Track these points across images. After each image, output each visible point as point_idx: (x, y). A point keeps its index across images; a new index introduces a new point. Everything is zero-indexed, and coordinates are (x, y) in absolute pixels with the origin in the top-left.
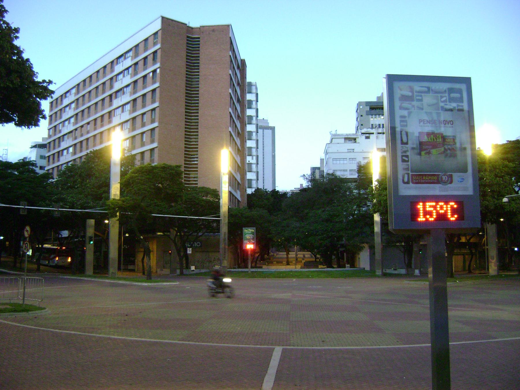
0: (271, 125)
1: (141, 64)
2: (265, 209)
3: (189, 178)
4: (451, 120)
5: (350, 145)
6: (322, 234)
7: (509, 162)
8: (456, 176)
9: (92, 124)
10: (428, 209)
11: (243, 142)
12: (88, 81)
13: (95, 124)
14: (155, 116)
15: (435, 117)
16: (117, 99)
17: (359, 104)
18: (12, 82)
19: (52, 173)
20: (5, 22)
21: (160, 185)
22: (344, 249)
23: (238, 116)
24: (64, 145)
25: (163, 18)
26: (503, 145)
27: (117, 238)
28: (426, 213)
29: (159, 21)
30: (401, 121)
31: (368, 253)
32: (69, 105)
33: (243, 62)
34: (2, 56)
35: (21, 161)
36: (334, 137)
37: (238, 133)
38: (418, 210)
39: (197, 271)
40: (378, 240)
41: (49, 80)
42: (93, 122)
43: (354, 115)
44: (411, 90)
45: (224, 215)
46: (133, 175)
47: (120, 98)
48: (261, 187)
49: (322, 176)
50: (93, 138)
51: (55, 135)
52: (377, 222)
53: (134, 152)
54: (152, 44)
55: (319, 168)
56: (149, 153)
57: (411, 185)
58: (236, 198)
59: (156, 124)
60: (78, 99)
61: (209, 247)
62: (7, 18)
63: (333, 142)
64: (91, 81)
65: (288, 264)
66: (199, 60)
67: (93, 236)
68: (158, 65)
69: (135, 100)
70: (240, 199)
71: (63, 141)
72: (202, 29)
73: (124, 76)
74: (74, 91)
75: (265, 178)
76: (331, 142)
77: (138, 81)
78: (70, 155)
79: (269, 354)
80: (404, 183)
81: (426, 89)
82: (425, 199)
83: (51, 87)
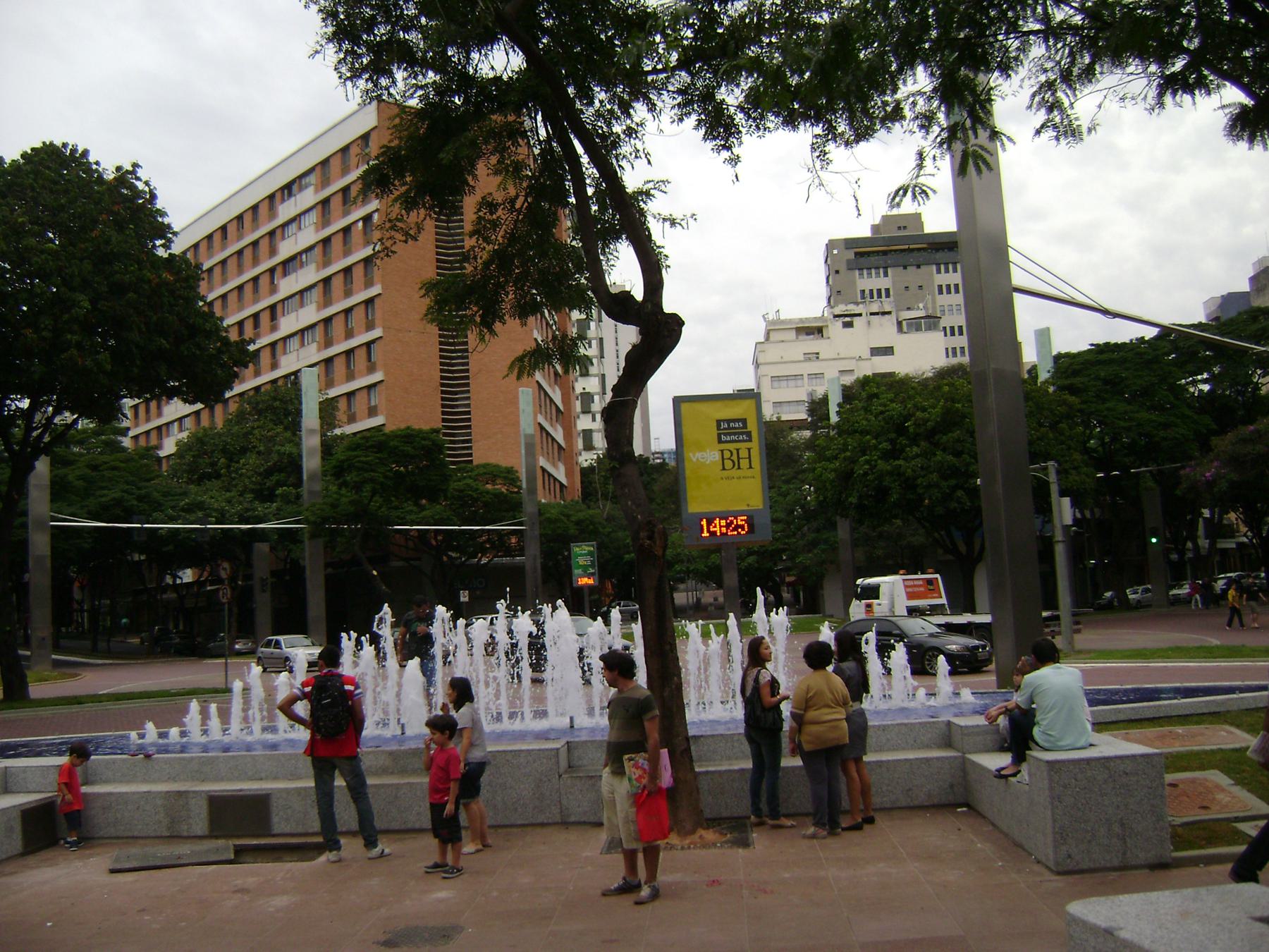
5: (812, 344)
16: (288, 278)
17: (831, 245)
36: (774, 328)
38: (702, 526)
43: (820, 272)
53: (333, 393)
58: (555, 479)
63: (772, 339)
70: (564, 481)
77: (261, 242)
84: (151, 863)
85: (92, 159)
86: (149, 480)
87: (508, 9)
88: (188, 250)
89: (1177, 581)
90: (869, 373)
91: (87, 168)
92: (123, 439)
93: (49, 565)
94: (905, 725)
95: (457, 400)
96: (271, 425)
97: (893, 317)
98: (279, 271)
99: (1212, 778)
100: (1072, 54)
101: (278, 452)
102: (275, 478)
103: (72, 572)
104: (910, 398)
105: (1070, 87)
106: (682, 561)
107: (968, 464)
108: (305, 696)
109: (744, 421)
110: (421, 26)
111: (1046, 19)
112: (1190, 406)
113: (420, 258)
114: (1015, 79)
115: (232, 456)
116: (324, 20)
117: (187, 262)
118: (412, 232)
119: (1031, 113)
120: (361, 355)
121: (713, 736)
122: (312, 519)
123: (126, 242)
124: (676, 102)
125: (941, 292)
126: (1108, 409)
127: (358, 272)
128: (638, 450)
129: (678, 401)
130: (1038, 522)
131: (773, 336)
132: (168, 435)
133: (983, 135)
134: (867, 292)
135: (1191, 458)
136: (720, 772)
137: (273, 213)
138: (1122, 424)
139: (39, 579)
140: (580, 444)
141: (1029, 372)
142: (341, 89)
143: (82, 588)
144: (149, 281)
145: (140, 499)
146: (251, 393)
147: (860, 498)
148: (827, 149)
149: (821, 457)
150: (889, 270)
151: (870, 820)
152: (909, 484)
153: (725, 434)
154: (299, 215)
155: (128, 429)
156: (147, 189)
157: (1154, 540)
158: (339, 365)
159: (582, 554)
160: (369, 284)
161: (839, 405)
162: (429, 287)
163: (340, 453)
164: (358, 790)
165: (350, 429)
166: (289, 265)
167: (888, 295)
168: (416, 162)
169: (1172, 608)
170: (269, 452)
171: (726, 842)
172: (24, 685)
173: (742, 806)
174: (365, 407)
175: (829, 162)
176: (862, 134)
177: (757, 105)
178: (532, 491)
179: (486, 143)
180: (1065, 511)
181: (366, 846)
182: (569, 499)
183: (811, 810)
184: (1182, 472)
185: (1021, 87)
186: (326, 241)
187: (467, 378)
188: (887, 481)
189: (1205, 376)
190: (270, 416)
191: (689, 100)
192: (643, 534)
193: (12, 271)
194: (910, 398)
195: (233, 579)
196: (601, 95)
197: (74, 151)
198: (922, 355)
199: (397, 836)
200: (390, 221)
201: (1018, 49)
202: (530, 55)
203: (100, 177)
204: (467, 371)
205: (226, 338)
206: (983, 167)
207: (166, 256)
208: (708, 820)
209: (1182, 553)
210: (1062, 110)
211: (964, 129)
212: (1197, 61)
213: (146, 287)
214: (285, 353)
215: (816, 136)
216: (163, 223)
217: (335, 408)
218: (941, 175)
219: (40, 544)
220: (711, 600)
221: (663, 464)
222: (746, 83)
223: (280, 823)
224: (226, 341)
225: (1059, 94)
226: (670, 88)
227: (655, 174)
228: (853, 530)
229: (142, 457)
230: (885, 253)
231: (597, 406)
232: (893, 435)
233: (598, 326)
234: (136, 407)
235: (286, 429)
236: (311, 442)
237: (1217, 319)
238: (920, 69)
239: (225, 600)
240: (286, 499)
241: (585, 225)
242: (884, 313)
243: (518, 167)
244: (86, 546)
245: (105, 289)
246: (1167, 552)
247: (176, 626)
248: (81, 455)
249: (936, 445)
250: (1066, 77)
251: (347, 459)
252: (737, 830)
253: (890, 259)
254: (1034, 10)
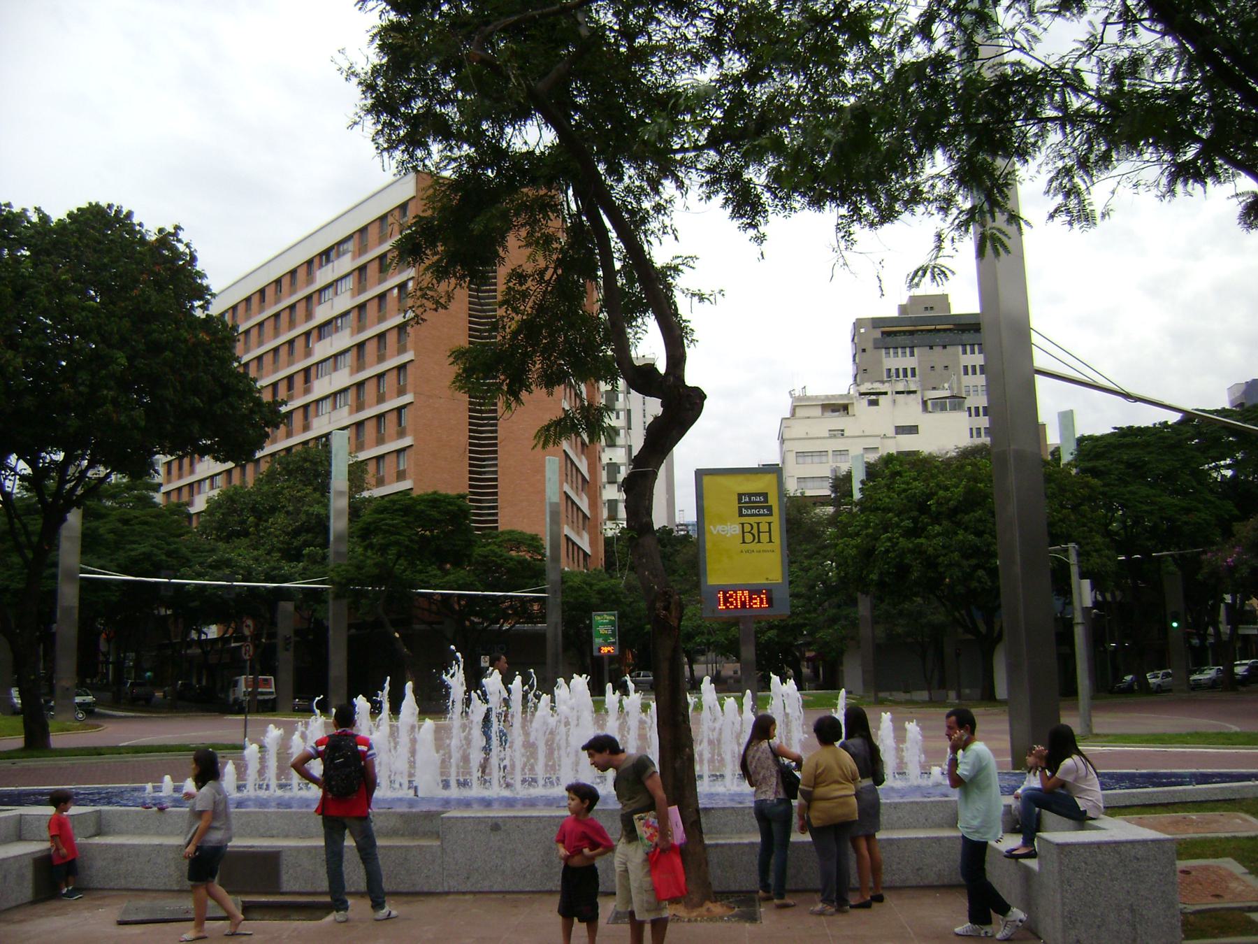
5: (837, 421)
14: (405, 380)
16: (323, 342)
17: (858, 324)
36: (800, 404)
43: (847, 349)
53: (362, 456)
58: (579, 548)
70: (588, 551)
76: (793, 414)
84: (159, 917)
85: (136, 220)
86: (182, 535)
87: (540, 86)
88: (226, 311)
89: (1199, 665)
90: (893, 451)
91: (131, 229)
92: (155, 495)
93: (76, 616)
94: (917, 803)
95: (484, 466)
96: (300, 486)
97: (918, 397)
98: (314, 334)
99: (1227, 866)
100: (1089, 141)
101: (307, 512)
102: (302, 538)
103: (99, 624)
104: (933, 476)
105: (1087, 173)
106: (703, 633)
107: (989, 545)
108: (319, 754)
109: (765, 495)
110: (458, 101)
111: (1063, 106)
112: (1211, 491)
113: (453, 325)
114: (1032, 165)
115: (261, 514)
116: (364, 92)
117: (225, 324)
118: (442, 301)
119: (1048, 198)
120: (391, 419)
121: (724, 809)
122: (337, 579)
123: (165, 302)
124: (703, 180)
125: (966, 373)
126: (1130, 492)
127: (392, 339)
128: (659, 520)
129: (700, 474)
130: (1058, 604)
131: (799, 412)
132: (199, 493)
133: (1001, 219)
134: (893, 371)
135: (1213, 544)
136: (730, 845)
137: (310, 278)
138: (1145, 508)
139: (66, 629)
140: (604, 476)
141: (1052, 454)
142: (378, 159)
143: (108, 640)
144: (186, 341)
145: (169, 554)
146: (282, 454)
147: (881, 574)
148: (852, 230)
149: (843, 533)
150: (916, 350)
151: (879, 899)
152: (930, 563)
153: (747, 508)
154: (337, 281)
155: (160, 485)
156: (187, 251)
157: (1175, 625)
158: (370, 429)
159: (603, 623)
160: (402, 350)
161: (862, 482)
162: (458, 355)
163: (367, 516)
164: (367, 851)
165: (378, 492)
166: (324, 329)
167: (913, 375)
168: (449, 232)
169: (1193, 693)
170: (298, 511)
171: (733, 916)
172: (45, 734)
173: (751, 881)
174: (393, 472)
175: (853, 243)
176: (887, 215)
177: (783, 185)
178: (556, 558)
179: (517, 214)
180: (1085, 593)
181: (373, 907)
182: (592, 567)
183: (820, 887)
184: (1204, 557)
185: (1038, 172)
186: (361, 307)
187: (495, 445)
188: (908, 560)
189: (1228, 461)
190: (299, 477)
191: (716, 178)
192: (659, 605)
193: (53, 327)
194: (933, 476)
195: (256, 637)
196: (630, 171)
197: (118, 212)
198: (947, 434)
199: (405, 899)
200: (421, 289)
201: (1036, 135)
202: (561, 132)
203: (143, 237)
204: (496, 438)
205: (259, 399)
206: (1001, 250)
207: (203, 316)
208: (716, 893)
209: (1203, 638)
210: (1078, 194)
211: (982, 212)
212: (1210, 149)
213: (183, 346)
214: (317, 415)
215: (842, 217)
216: (201, 285)
217: (364, 471)
218: (963, 255)
219: (69, 595)
220: (731, 673)
221: (687, 536)
222: (771, 162)
223: (289, 881)
224: (258, 402)
225: (1076, 180)
226: (699, 166)
227: (683, 249)
228: (874, 607)
229: (173, 513)
230: (912, 333)
231: (621, 477)
232: (915, 513)
233: (626, 398)
234: (169, 464)
235: (315, 490)
236: (339, 504)
237: (1241, 405)
238: (939, 153)
239: (247, 657)
240: (313, 559)
241: (613, 297)
242: (910, 392)
243: (548, 240)
244: (113, 598)
245: (141, 347)
246: (1188, 637)
247: (199, 681)
248: (113, 509)
249: (958, 524)
250: (1083, 163)
251: (373, 522)
252: (744, 904)
253: (916, 339)
254: (1052, 98)
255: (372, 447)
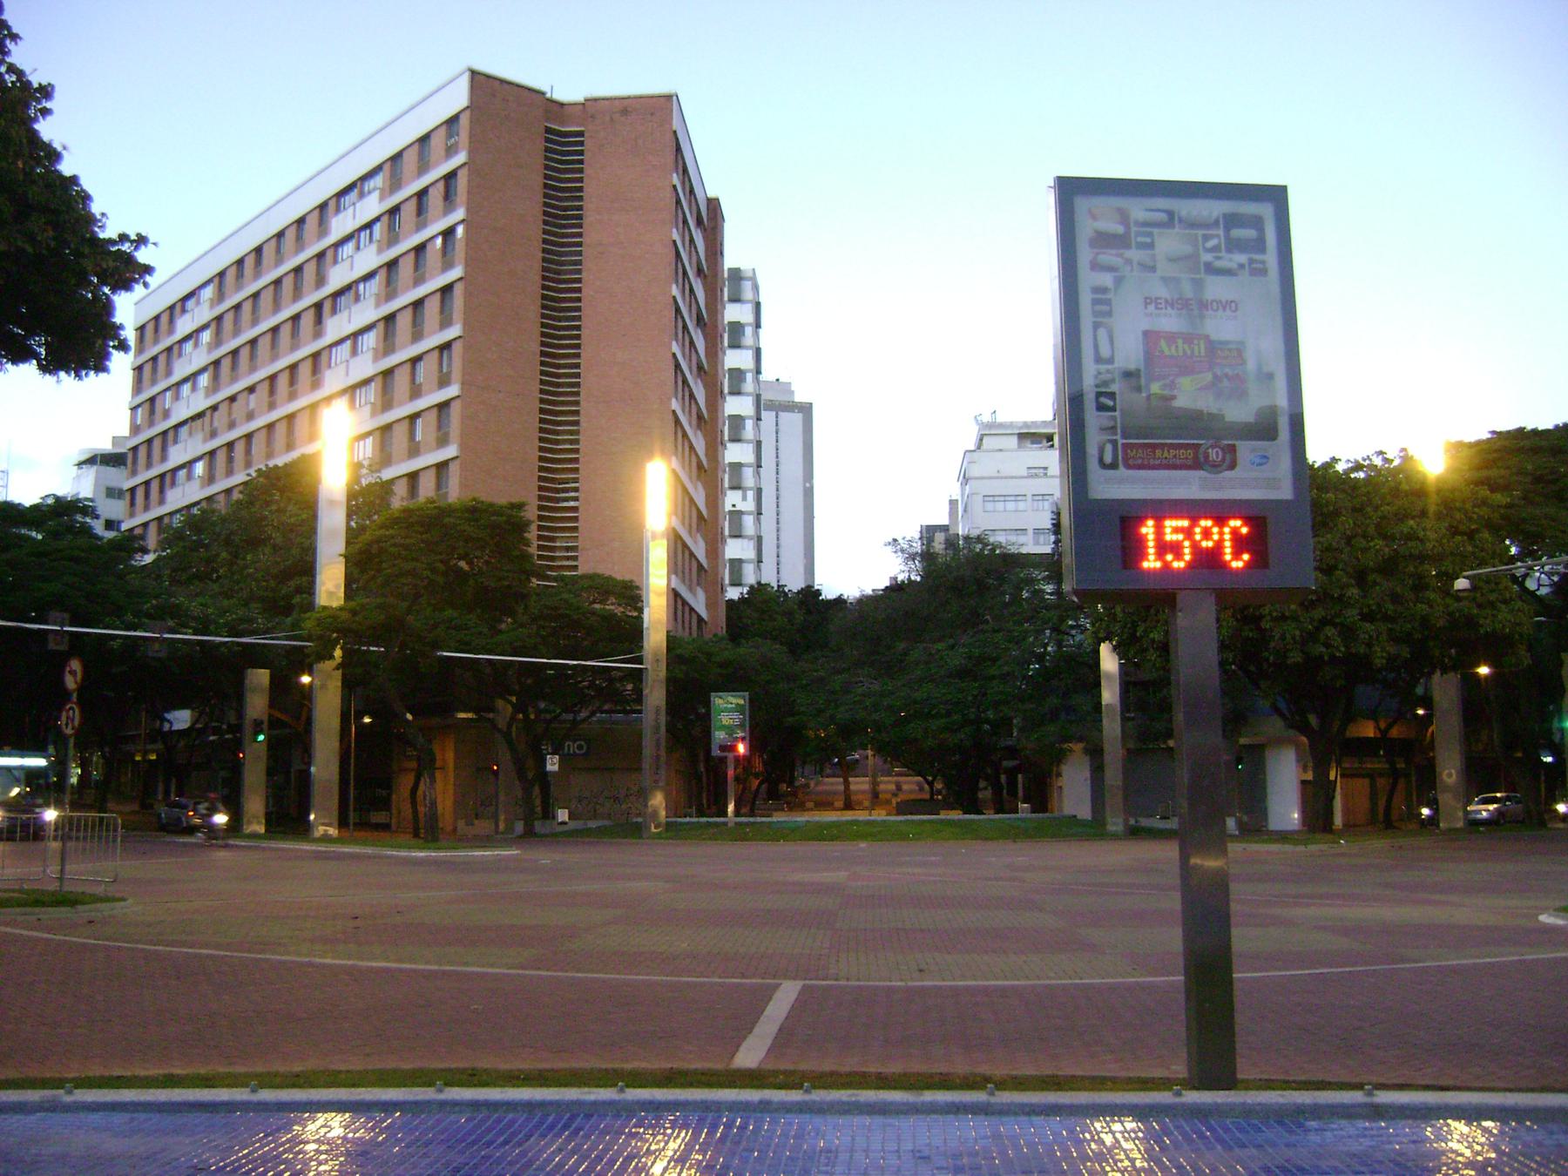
0: (799, 398)
1: (409, 210)
2: (786, 632)
3: (553, 549)
4: (1230, 298)
6: (949, 714)
7: (1492, 491)
8: (1245, 449)
9: (263, 390)
10: (1170, 537)
11: (715, 446)
12: (249, 263)
13: (272, 392)
14: (449, 365)
15: (1188, 292)
18: (32, 239)
19: (143, 537)
20: (12, 69)
21: (463, 564)
22: (1015, 763)
23: (700, 368)
24: (177, 455)
25: (474, 74)
26: (1479, 443)
27: (336, 723)
28: (1163, 548)
29: (464, 84)
30: (1095, 302)
31: (1087, 774)
32: (193, 336)
33: (714, 205)
34: (4, 164)
35: (50, 501)
36: (988, 431)
37: (700, 417)
38: (1141, 541)
39: (573, 825)
40: (1112, 727)
41: (138, 235)
42: (267, 383)
44: (1124, 218)
45: (656, 654)
46: (382, 532)
47: (345, 314)
48: (769, 577)
49: (951, 543)
50: (264, 432)
51: (151, 424)
52: (1109, 676)
53: (387, 474)
54: (443, 153)
55: (944, 528)
56: (432, 473)
57: (1122, 471)
58: (692, 609)
59: (453, 391)
60: (219, 319)
61: (613, 756)
62: (18, 55)
64: (258, 262)
65: (849, 806)
66: (580, 198)
67: (265, 718)
68: (460, 214)
69: (390, 319)
70: (704, 615)
71: (176, 442)
72: (591, 107)
73: (358, 248)
74: (208, 293)
75: (782, 559)
76: (979, 447)
78: (196, 484)
79: (766, 995)
80: (1103, 465)
81: (1163, 217)
82: (1161, 510)
83: (142, 256)
239: (69, 731)
255: (403, 460)
